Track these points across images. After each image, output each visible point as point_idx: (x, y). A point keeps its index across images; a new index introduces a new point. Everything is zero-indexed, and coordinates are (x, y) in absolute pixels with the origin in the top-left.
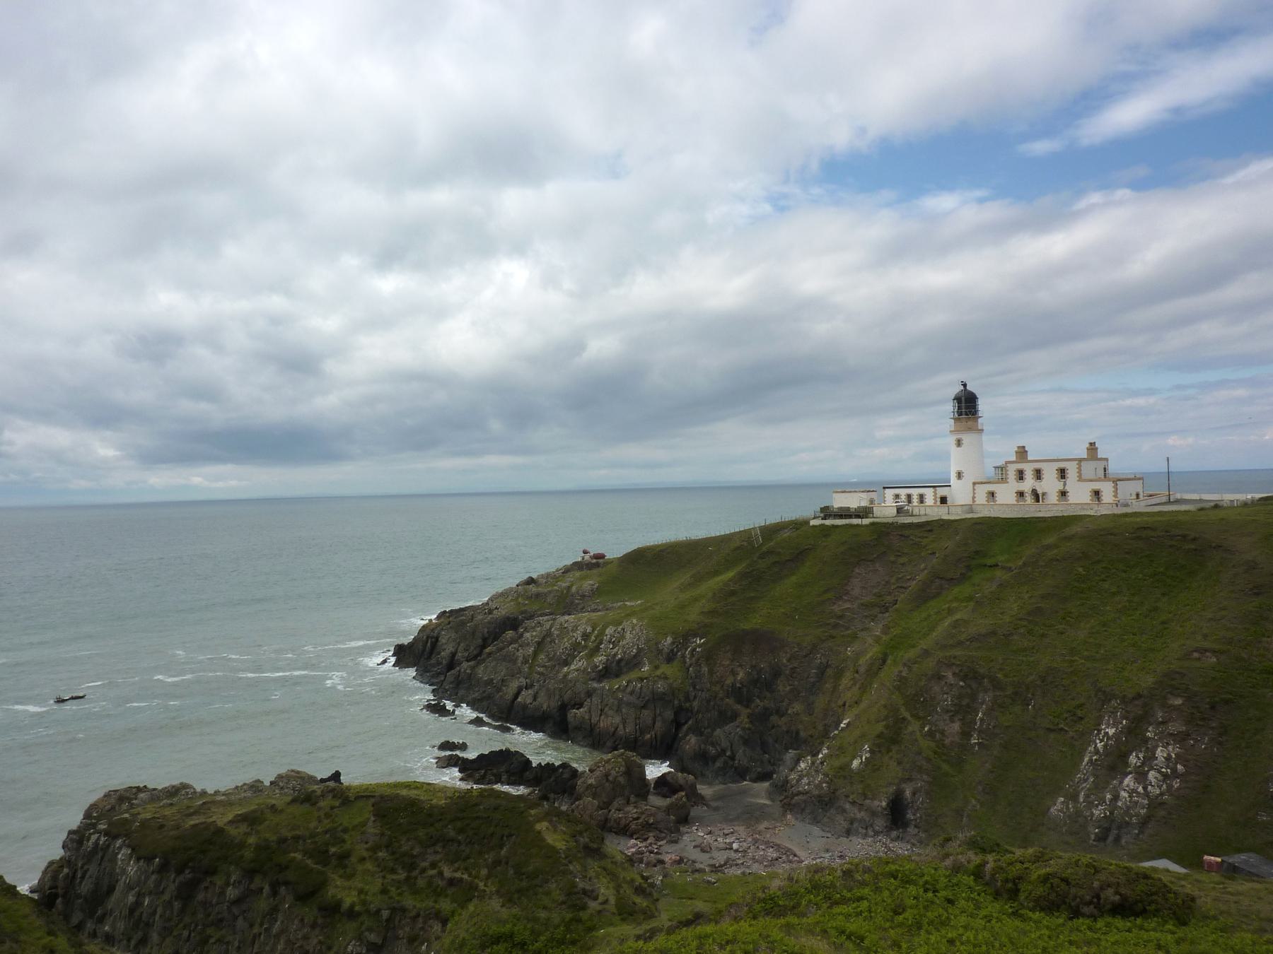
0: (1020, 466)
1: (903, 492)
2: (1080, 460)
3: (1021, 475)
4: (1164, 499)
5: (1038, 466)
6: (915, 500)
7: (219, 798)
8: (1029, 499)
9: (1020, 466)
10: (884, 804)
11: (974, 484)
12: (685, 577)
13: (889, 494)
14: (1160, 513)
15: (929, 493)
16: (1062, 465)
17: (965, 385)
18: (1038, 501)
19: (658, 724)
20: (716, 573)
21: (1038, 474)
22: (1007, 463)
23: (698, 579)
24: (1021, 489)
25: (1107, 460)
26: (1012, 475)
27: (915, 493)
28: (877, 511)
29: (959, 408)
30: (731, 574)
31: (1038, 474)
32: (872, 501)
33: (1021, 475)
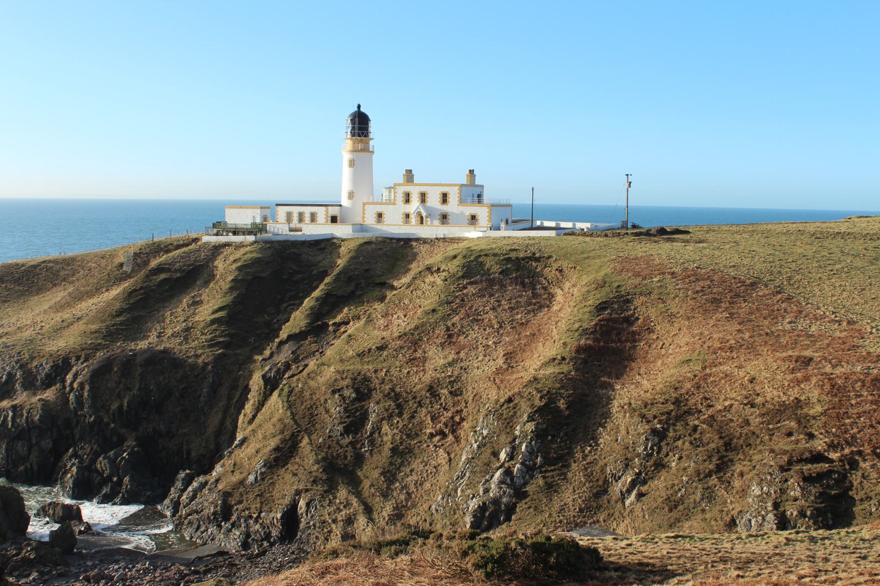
0: (408, 188)
1: (296, 210)
2: (462, 185)
3: (407, 199)
4: (528, 225)
5: (423, 189)
6: (307, 218)
7: (657, 578)
8: (414, 219)
9: (408, 188)
10: (279, 515)
11: (364, 204)
12: (59, 295)
13: (282, 212)
14: (530, 238)
15: (321, 212)
16: (445, 189)
17: (359, 107)
18: (422, 223)
19: (33, 457)
20: (97, 290)
21: (423, 197)
22: (395, 185)
23: (79, 297)
24: (407, 211)
25: (482, 186)
26: (400, 198)
27: (307, 210)
28: (270, 226)
29: (353, 128)
30: (115, 291)
31: (423, 197)
32: (265, 219)
33: (407, 199)
